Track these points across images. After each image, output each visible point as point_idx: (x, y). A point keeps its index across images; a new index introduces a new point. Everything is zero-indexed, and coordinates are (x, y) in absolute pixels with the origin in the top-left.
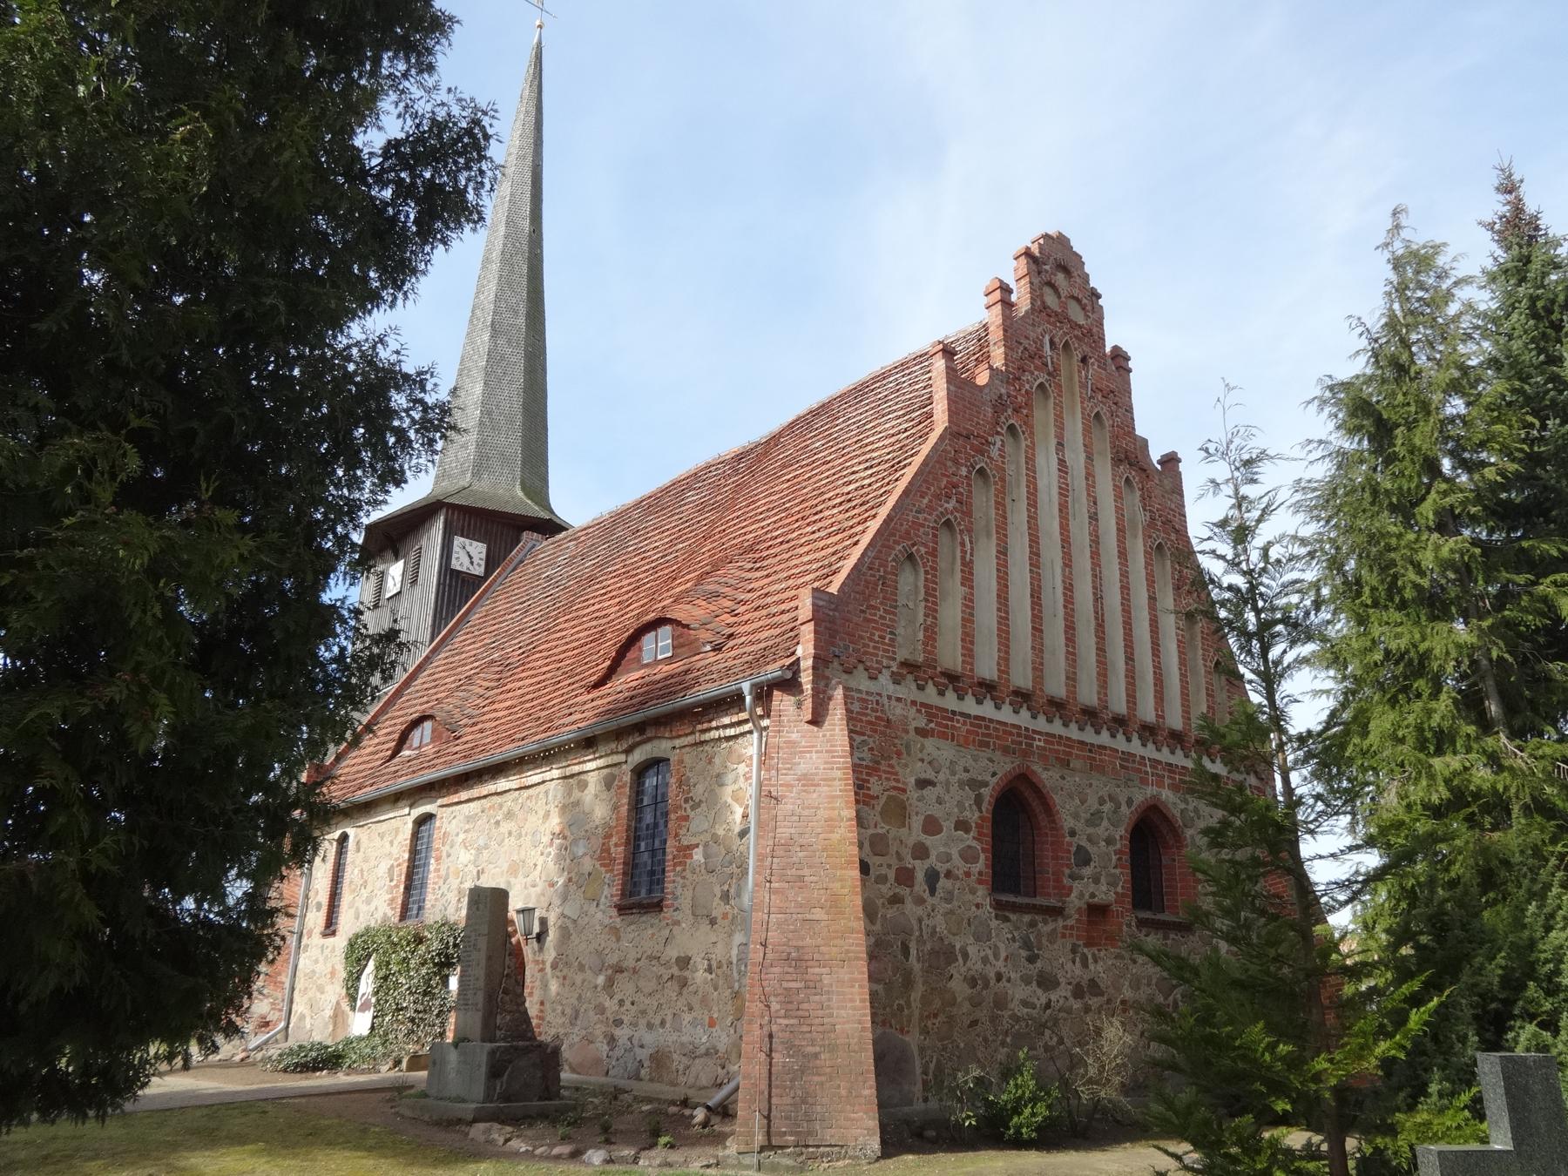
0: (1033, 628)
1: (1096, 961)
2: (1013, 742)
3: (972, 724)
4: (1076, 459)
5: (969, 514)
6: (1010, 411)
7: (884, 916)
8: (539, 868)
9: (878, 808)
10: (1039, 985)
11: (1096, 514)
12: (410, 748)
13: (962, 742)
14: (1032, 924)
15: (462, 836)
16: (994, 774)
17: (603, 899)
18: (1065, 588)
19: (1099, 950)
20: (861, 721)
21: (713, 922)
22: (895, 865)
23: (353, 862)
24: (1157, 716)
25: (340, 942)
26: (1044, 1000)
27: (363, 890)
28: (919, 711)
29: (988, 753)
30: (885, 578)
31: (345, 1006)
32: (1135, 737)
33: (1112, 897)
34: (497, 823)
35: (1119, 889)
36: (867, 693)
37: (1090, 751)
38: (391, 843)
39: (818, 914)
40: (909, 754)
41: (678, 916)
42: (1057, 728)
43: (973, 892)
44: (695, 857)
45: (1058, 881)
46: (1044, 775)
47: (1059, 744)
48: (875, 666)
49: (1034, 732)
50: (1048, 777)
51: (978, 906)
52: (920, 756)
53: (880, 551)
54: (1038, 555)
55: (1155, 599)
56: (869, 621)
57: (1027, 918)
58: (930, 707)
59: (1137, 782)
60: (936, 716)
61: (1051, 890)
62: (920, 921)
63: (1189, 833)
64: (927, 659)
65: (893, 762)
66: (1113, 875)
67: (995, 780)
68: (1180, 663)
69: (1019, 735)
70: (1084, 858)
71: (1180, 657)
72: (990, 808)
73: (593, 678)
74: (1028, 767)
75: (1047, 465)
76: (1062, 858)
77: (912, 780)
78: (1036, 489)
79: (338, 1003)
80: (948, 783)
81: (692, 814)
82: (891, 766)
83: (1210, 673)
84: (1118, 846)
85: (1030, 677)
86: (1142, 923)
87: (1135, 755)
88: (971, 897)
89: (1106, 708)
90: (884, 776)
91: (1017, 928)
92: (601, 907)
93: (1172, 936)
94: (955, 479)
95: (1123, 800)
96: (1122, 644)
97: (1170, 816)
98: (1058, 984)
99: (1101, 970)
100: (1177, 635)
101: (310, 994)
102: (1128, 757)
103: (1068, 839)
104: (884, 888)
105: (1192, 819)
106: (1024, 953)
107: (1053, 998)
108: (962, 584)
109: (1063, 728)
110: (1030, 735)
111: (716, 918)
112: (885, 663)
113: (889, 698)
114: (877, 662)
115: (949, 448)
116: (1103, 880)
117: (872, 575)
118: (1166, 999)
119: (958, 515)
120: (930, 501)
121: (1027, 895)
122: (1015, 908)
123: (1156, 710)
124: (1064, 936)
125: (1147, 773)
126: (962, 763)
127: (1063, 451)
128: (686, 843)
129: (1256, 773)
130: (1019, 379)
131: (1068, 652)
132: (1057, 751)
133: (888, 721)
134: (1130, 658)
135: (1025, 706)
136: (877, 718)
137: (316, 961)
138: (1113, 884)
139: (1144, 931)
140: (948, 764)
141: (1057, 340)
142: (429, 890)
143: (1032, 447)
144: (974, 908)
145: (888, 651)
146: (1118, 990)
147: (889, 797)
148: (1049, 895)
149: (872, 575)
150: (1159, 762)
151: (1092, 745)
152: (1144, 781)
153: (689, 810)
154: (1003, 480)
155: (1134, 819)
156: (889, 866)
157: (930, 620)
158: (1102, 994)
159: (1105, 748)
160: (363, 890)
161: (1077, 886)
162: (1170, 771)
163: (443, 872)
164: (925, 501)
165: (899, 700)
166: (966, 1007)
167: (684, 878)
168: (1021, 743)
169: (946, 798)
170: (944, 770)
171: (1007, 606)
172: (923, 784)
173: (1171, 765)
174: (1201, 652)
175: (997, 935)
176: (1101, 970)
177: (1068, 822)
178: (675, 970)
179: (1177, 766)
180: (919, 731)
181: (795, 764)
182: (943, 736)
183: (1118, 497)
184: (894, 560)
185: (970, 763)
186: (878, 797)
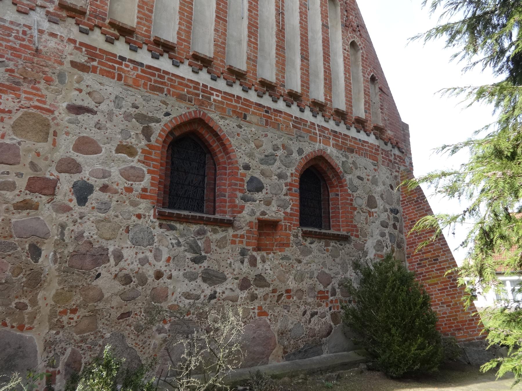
0: (217, 16)
1: (264, 261)
2: (188, 92)
3: (142, 71)
10: (205, 280)
13: (130, 82)
14: (201, 233)
16: (167, 114)
19: (268, 254)
22: (29, 173)
24: (326, 99)
26: (208, 292)
29: (162, 97)
33: (281, 215)
35: (288, 210)
42: (237, 90)
43: (134, 204)
45: (232, 201)
46: (221, 123)
51: (139, 216)
52: (77, 86)
55: (327, 27)
57: (194, 228)
59: (307, 139)
62: (63, 227)
63: (348, 177)
68: (345, 70)
71: (345, 67)
77: (65, 105)
80: (110, 115)
83: (367, 81)
84: (289, 180)
85: (212, 51)
86: (306, 235)
87: (307, 121)
88: (131, 209)
90: (23, 95)
91: (182, 235)
93: (332, 244)
96: (300, 48)
97: (334, 165)
98: (225, 279)
99: (268, 268)
100: (344, 53)
102: (299, 121)
103: (242, 171)
106: (190, 255)
107: (219, 290)
109: (192, 74)
116: (274, 203)
118: (325, 287)
122: (181, 219)
124: (233, 242)
125: (316, 134)
126: (130, 100)
129: (399, 148)
132: (236, 107)
133: (37, 50)
134: (305, 58)
135: (267, 93)
139: (309, 240)
144: (134, 218)
146: (283, 282)
150: (327, 129)
152: (313, 139)
155: (303, 163)
158: (269, 286)
159: (281, 112)
162: (334, 136)
166: (116, 301)
168: (198, 95)
169: (108, 125)
173: (336, 132)
174: (361, 68)
175: (160, 241)
176: (268, 268)
179: (340, 134)
185: (140, 101)
186: (10, 112)
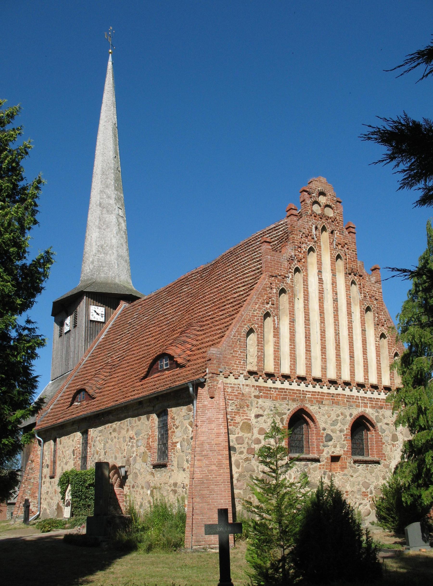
2: (297, 396)
4: (327, 276)
5: (277, 308)
6: (296, 262)
7: (242, 466)
8: (126, 450)
9: (239, 427)
11: (337, 299)
12: (77, 402)
13: (274, 399)
14: (307, 465)
15: (98, 438)
16: (289, 410)
17: (148, 462)
18: (321, 332)
20: (232, 395)
21: (184, 470)
23: (59, 448)
24: (365, 379)
25: (57, 480)
27: (64, 460)
28: (256, 389)
29: (286, 402)
30: (240, 339)
31: (61, 504)
32: (354, 389)
34: (110, 433)
35: (346, 449)
36: (234, 384)
37: (332, 396)
38: (73, 441)
39: (214, 467)
40: (252, 405)
41: (173, 468)
44: (177, 446)
45: (318, 447)
47: (318, 395)
48: (237, 374)
49: (306, 391)
50: (312, 409)
52: (256, 406)
53: (238, 329)
54: (309, 320)
56: (234, 357)
58: (260, 387)
59: (354, 407)
60: (263, 390)
61: (315, 451)
64: (258, 369)
65: (246, 409)
66: (343, 444)
67: (289, 411)
69: (300, 393)
70: (329, 438)
72: (287, 423)
73: (143, 375)
74: (304, 405)
75: (313, 280)
76: (319, 439)
78: (308, 293)
79: (58, 503)
81: (176, 430)
82: (244, 411)
84: (345, 432)
87: (354, 396)
89: (340, 378)
90: (241, 415)
92: (148, 465)
94: (270, 295)
95: (348, 414)
101: (47, 500)
103: (322, 432)
104: (243, 456)
105: (381, 419)
108: (274, 337)
110: (304, 393)
111: (185, 469)
112: (241, 372)
113: (243, 385)
114: (238, 372)
115: (267, 282)
116: (338, 446)
117: (235, 339)
118: (366, 490)
119: (272, 309)
120: (259, 306)
121: (307, 454)
123: (365, 376)
125: (359, 403)
127: (321, 275)
128: (174, 441)
130: (300, 247)
131: (322, 358)
132: (317, 398)
136: (238, 393)
137: (49, 488)
138: (342, 447)
139: (357, 464)
140: (268, 408)
141: (319, 226)
142: (88, 459)
143: (307, 276)
145: (242, 367)
147: (244, 423)
148: (314, 453)
149: (235, 339)
150: (366, 398)
151: (334, 394)
152: (358, 406)
153: (175, 429)
154: (292, 291)
156: (244, 448)
157: (260, 353)
159: (339, 394)
160: (64, 460)
161: (326, 449)
162: (370, 401)
163: (93, 452)
164: (257, 306)
165: (247, 385)
167: (174, 454)
170: (267, 410)
171: (294, 343)
172: (257, 416)
173: (371, 398)
177: (322, 425)
178: (173, 488)
179: (374, 398)
180: (255, 396)
181: (206, 413)
182: (266, 397)
183: (348, 289)
184: (244, 332)
186: (239, 423)
